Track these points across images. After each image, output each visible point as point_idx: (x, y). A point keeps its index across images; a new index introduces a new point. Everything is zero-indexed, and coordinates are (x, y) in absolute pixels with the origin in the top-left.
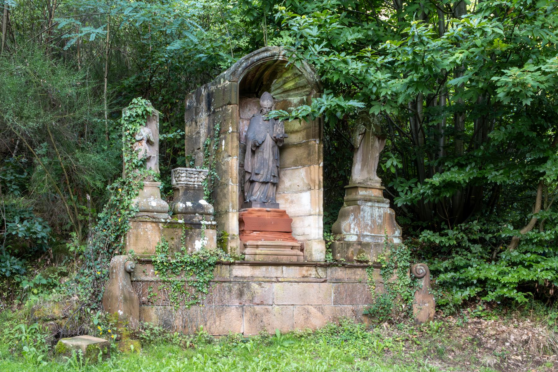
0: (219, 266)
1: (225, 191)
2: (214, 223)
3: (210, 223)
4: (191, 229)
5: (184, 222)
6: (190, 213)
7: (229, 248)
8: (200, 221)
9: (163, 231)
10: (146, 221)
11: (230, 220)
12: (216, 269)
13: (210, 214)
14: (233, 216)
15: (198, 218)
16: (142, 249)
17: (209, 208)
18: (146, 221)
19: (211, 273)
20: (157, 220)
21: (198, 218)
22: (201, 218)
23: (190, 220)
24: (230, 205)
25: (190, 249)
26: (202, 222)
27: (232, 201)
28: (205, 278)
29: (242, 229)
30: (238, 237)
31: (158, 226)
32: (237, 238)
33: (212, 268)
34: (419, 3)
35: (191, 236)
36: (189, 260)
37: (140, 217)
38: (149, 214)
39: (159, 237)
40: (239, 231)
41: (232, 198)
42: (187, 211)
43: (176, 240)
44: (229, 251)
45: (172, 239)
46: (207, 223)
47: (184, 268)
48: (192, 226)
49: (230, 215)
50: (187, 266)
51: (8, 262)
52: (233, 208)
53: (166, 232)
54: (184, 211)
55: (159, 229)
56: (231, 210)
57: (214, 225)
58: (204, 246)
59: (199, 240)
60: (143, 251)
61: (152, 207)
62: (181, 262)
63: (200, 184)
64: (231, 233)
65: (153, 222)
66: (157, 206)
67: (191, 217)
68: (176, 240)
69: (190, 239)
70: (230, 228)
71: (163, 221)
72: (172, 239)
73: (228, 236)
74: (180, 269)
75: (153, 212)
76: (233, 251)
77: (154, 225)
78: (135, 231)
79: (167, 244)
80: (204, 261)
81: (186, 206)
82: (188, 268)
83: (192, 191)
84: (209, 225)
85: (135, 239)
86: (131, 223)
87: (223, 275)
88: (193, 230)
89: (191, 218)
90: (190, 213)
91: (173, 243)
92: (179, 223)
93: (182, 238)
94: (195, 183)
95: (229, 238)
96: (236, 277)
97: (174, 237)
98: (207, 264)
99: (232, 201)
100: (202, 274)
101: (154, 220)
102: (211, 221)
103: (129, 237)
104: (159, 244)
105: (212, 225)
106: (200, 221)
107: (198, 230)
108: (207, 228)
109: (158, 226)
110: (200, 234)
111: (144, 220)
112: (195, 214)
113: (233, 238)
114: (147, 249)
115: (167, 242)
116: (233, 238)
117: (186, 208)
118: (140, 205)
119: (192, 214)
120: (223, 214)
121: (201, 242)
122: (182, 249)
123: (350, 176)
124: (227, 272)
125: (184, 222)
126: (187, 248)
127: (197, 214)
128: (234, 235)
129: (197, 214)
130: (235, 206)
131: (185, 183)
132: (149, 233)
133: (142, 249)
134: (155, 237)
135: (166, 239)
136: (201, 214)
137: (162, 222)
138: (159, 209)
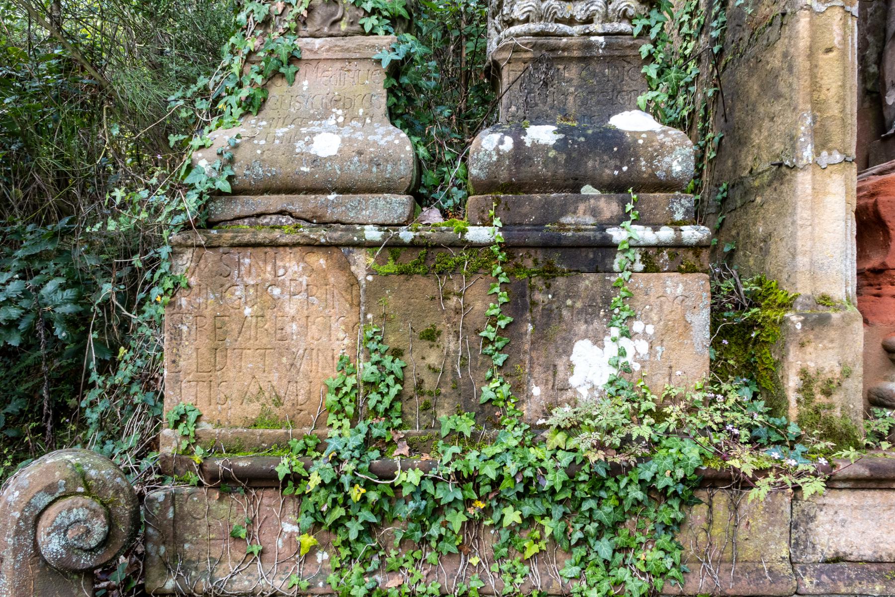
0: (721, 498)
1: (775, 60)
2: (692, 234)
3: (666, 234)
4: (549, 273)
5: (499, 237)
6: (543, 185)
7: (792, 382)
8: (602, 227)
9: (374, 292)
10: (274, 245)
11: (802, 214)
12: (698, 513)
13: (669, 185)
14: (818, 192)
15: (594, 212)
16: (244, 397)
17: (663, 150)
18: (274, 245)
19: (664, 540)
20: (337, 235)
21: (594, 212)
22: (609, 207)
23: (538, 225)
24: (804, 127)
25: (536, 391)
26: (617, 235)
27: (817, 105)
28: (623, 574)
29: (875, 261)
30: (853, 310)
31: (345, 266)
32: (847, 321)
33: (670, 512)
34: (530, 465)
35: (550, 315)
36: (512, 468)
37: (245, 224)
38: (298, 203)
39: (351, 329)
40: (860, 274)
41: (815, 86)
42: (526, 172)
43: (450, 343)
44: (792, 396)
45: (431, 336)
46: (645, 235)
47: (487, 512)
48: (555, 257)
49: (804, 181)
50: (502, 501)
51: (266, 327)
52: (822, 143)
53: (390, 300)
54: (503, 176)
55: (353, 281)
56: (807, 153)
57: (697, 248)
58: (627, 370)
59: (598, 341)
60: (253, 410)
61: (315, 161)
62: (460, 479)
63: (624, 26)
64: (804, 288)
65: (312, 246)
66: (341, 157)
67: (548, 203)
68: (450, 343)
69: (542, 336)
70: (802, 261)
71: (372, 234)
72: (431, 336)
73: (786, 306)
74: (457, 520)
75: (325, 191)
76: (820, 399)
77: (319, 261)
78: (208, 302)
79: (397, 366)
80: (615, 471)
81: (519, 145)
82: (512, 516)
83: (572, 73)
84: (660, 247)
85: (204, 343)
86: (188, 254)
87: (749, 551)
88: (560, 282)
89: (551, 214)
90: (543, 185)
91: (433, 358)
92: (473, 247)
93: (489, 332)
94: (596, 27)
95: (794, 319)
96: (837, 559)
97: (443, 326)
98: (636, 493)
99: (817, 105)
100: (604, 548)
101: (322, 235)
102: (676, 225)
103: (177, 335)
104: (346, 366)
105: (678, 246)
106: (602, 227)
107: (588, 281)
108: (650, 267)
109: (345, 266)
110: (607, 301)
111: (262, 236)
112: (576, 189)
113: (823, 321)
114: (278, 402)
115: (397, 353)
116: (823, 321)
117: (521, 155)
118: (239, 156)
119: (559, 189)
120: (760, 189)
121: (611, 349)
122: (487, 392)
123: (780, 215)
124: (777, 531)
125: (499, 237)
126: (518, 388)
127: (587, 190)
128: (825, 300)
129: (587, 190)
130: (834, 128)
131: (535, 27)
132: (291, 308)
133: (244, 397)
134: (327, 328)
135: (392, 340)
136: (616, 187)
137: (372, 245)
138: (356, 170)
